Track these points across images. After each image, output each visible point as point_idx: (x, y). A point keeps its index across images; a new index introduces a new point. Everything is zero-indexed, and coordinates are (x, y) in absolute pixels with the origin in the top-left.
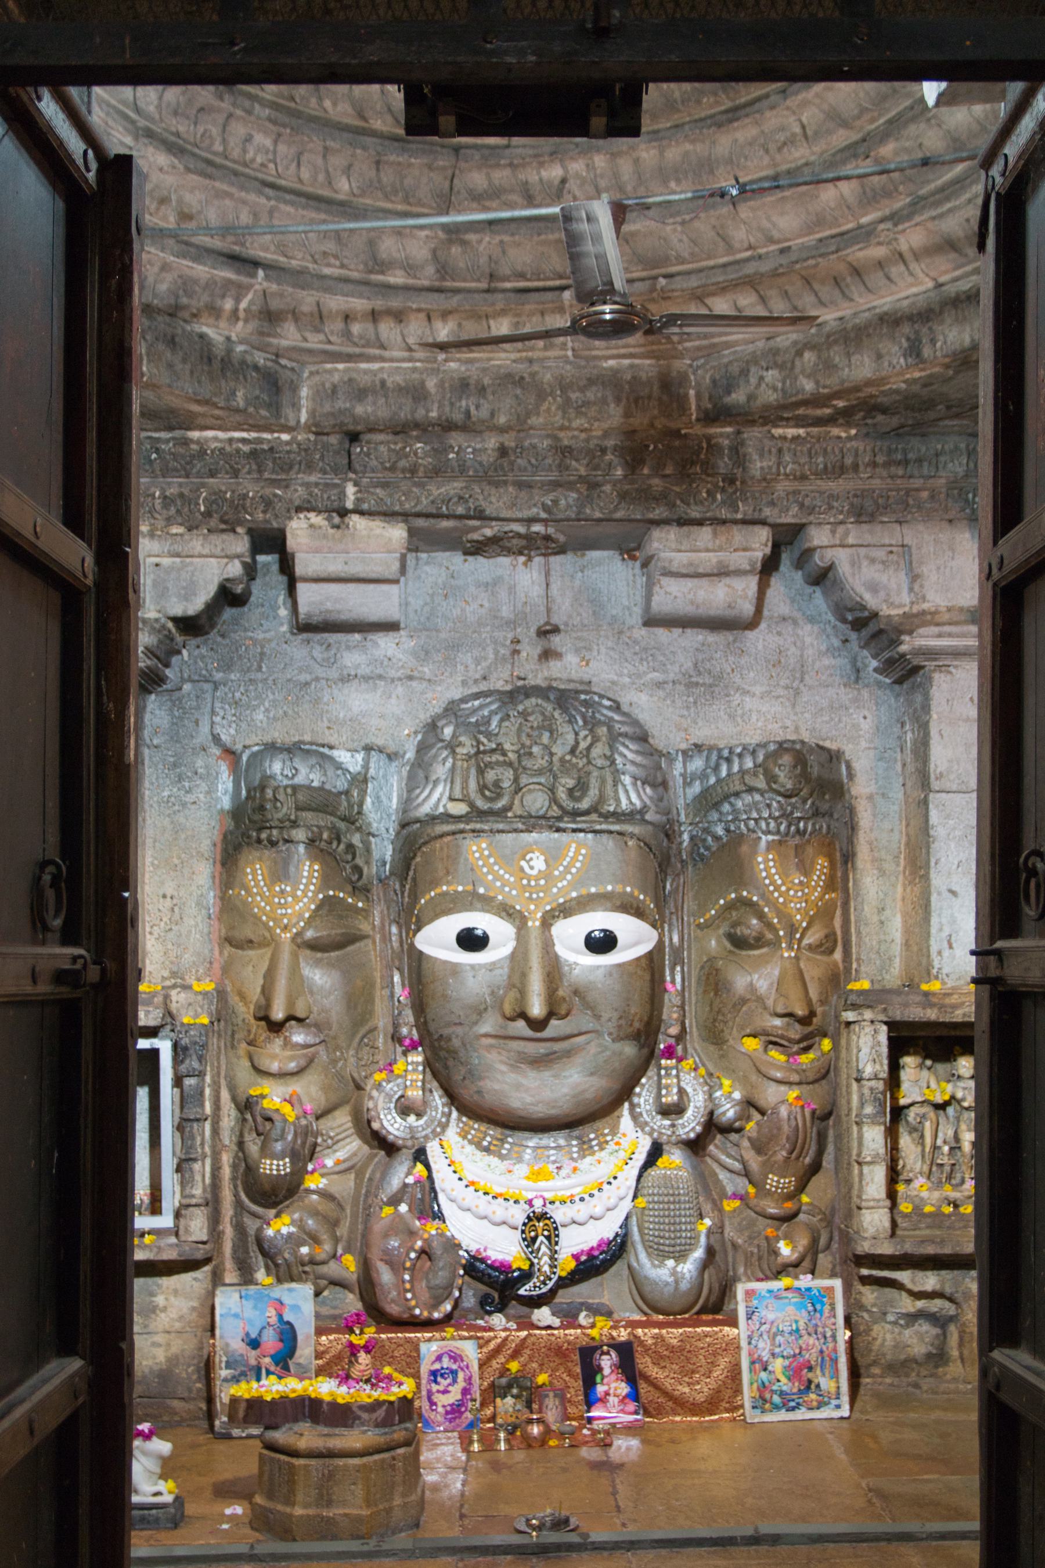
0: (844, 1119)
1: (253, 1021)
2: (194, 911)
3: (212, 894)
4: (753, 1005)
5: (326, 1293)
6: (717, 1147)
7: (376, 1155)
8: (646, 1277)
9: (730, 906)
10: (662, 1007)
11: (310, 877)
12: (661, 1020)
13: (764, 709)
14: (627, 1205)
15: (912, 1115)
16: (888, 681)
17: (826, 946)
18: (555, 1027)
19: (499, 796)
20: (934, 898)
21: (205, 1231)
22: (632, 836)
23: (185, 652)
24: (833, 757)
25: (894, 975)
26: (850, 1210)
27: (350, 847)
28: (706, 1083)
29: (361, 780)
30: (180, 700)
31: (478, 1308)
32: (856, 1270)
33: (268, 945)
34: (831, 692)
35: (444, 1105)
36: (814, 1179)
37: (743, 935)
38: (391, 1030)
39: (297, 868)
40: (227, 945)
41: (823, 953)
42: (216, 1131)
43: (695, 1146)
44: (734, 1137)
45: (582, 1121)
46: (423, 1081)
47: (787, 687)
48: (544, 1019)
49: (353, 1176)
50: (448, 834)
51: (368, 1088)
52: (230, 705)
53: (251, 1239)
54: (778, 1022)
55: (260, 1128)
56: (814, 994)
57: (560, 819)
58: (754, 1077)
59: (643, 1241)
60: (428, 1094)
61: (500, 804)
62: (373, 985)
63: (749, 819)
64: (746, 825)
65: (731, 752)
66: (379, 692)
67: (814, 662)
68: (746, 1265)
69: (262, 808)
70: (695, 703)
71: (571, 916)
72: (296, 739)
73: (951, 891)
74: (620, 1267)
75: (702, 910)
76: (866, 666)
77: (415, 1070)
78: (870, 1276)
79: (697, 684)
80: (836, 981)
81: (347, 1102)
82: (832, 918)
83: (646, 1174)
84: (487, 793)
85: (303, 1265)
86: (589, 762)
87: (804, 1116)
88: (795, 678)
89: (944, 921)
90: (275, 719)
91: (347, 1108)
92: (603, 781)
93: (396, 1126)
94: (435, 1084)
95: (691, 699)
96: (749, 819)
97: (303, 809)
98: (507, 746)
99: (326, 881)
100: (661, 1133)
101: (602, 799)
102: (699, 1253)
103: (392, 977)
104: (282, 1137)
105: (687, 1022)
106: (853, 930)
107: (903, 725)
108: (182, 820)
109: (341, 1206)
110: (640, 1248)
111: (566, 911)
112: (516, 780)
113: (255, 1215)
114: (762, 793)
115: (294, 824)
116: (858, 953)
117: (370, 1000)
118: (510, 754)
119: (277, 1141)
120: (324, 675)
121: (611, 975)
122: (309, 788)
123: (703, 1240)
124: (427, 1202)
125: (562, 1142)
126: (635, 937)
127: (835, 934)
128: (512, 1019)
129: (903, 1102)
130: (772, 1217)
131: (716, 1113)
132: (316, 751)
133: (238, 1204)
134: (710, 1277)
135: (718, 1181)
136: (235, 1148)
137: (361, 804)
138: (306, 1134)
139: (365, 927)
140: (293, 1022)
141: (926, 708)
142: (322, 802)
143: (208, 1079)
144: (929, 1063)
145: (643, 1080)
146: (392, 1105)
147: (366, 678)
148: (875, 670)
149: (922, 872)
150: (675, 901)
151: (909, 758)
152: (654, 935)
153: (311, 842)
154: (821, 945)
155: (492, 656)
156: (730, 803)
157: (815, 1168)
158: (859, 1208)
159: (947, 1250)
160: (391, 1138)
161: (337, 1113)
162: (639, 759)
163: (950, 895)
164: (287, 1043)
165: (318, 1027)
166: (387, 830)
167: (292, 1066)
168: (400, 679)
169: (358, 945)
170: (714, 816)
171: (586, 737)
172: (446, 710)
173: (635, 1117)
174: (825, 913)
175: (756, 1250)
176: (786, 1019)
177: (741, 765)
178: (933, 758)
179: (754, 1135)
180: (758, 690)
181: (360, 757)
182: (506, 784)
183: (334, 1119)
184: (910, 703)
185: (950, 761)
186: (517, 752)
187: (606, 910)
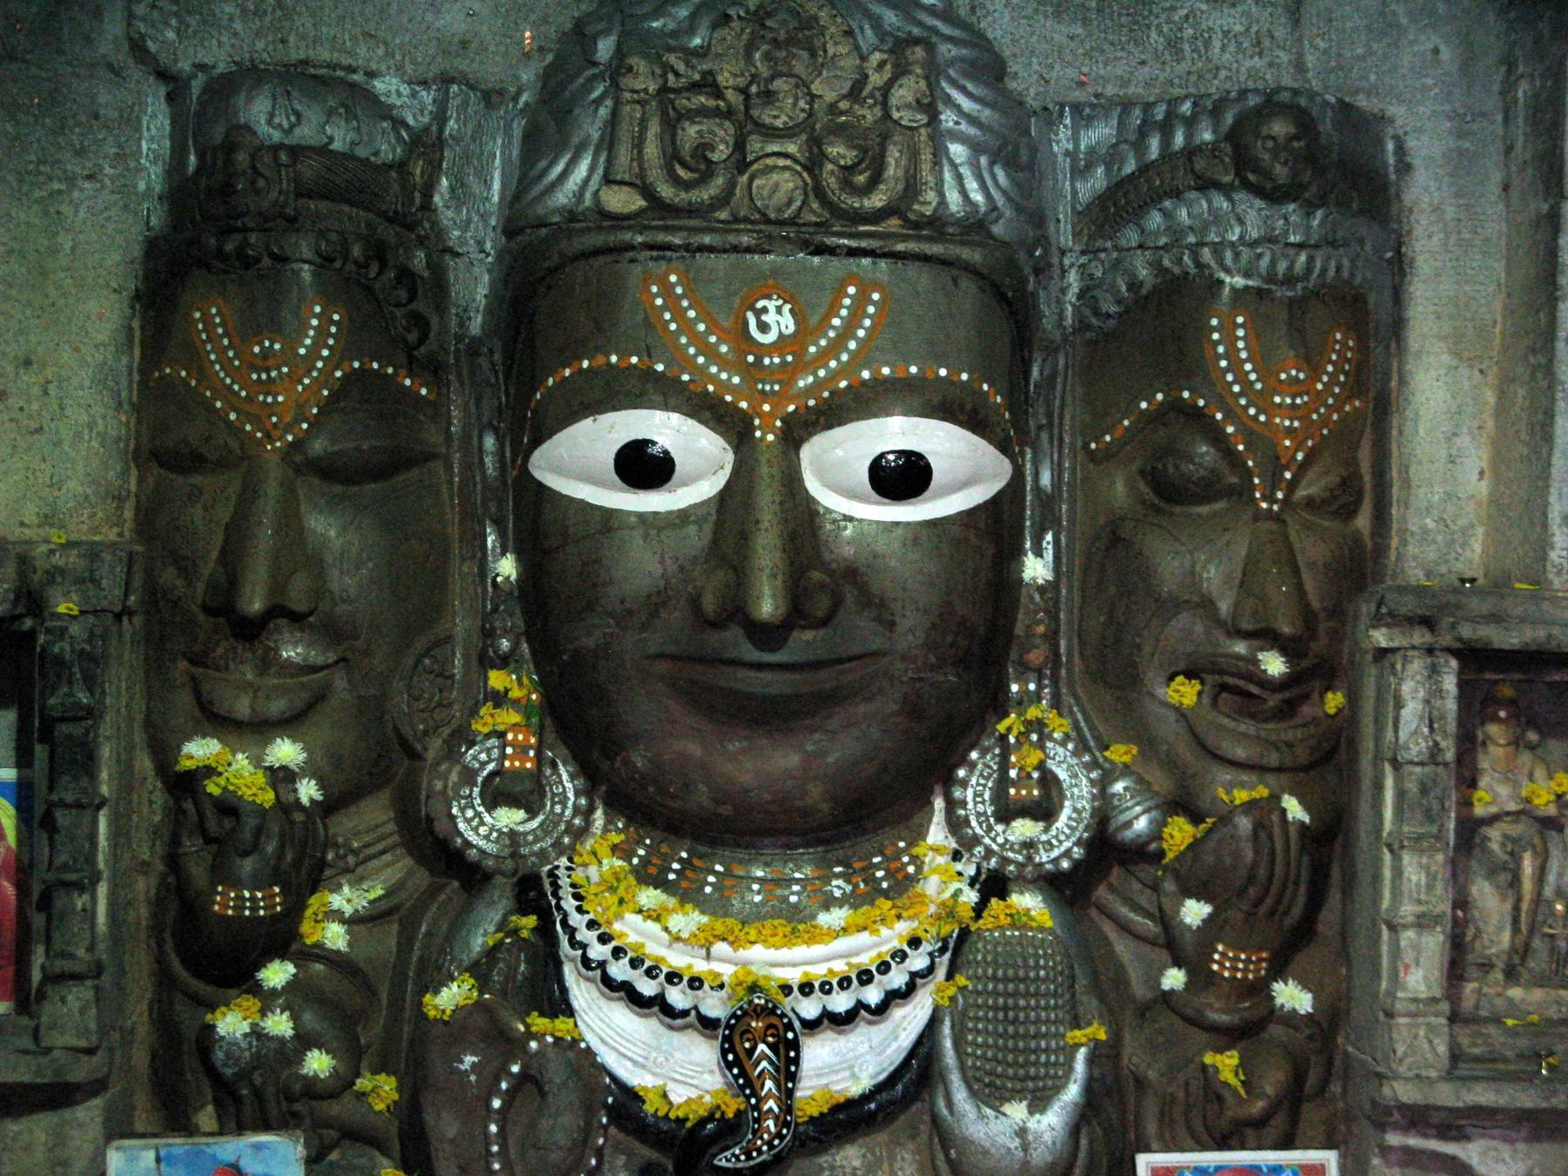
5: (334, 1156)
7: (441, 888)
9: (1157, 417)
10: (1015, 609)
11: (322, 332)
12: (1010, 636)
17: (1342, 502)
18: (803, 643)
19: (705, 177)
27: (406, 276)
29: (427, 145)
35: (577, 794)
39: (296, 312)
41: (1335, 514)
49: (395, 928)
50: (597, 252)
57: (822, 229)
59: (962, 1068)
61: (705, 194)
68: (1161, 1121)
69: (227, 190)
71: (841, 422)
72: (302, 56)
75: (1098, 421)
84: (681, 172)
86: (887, 116)
92: (914, 155)
97: (310, 195)
98: (724, 79)
99: (350, 345)
100: (1008, 861)
101: (912, 188)
109: (371, 990)
110: (955, 1080)
112: (740, 146)
118: (730, 95)
119: (246, 854)
121: (916, 541)
122: (323, 150)
129: (1479, 810)
131: (1113, 826)
132: (342, 80)
135: (1111, 954)
136: (160, 866)
137: (428, 192)
139: (433, 437)
140: (282, 622)
142: (349, 182)
146: (476, 790)
150: (1049, 404)
153: (324, 262)
156: (1167, 214)
162: (986, 114)
164: (268, 662)
166: (480, 243)
170: (1131, 236)
171: (881, 65)
174: (1342, 440)
177: (1189, 136)
182: (721, 153)
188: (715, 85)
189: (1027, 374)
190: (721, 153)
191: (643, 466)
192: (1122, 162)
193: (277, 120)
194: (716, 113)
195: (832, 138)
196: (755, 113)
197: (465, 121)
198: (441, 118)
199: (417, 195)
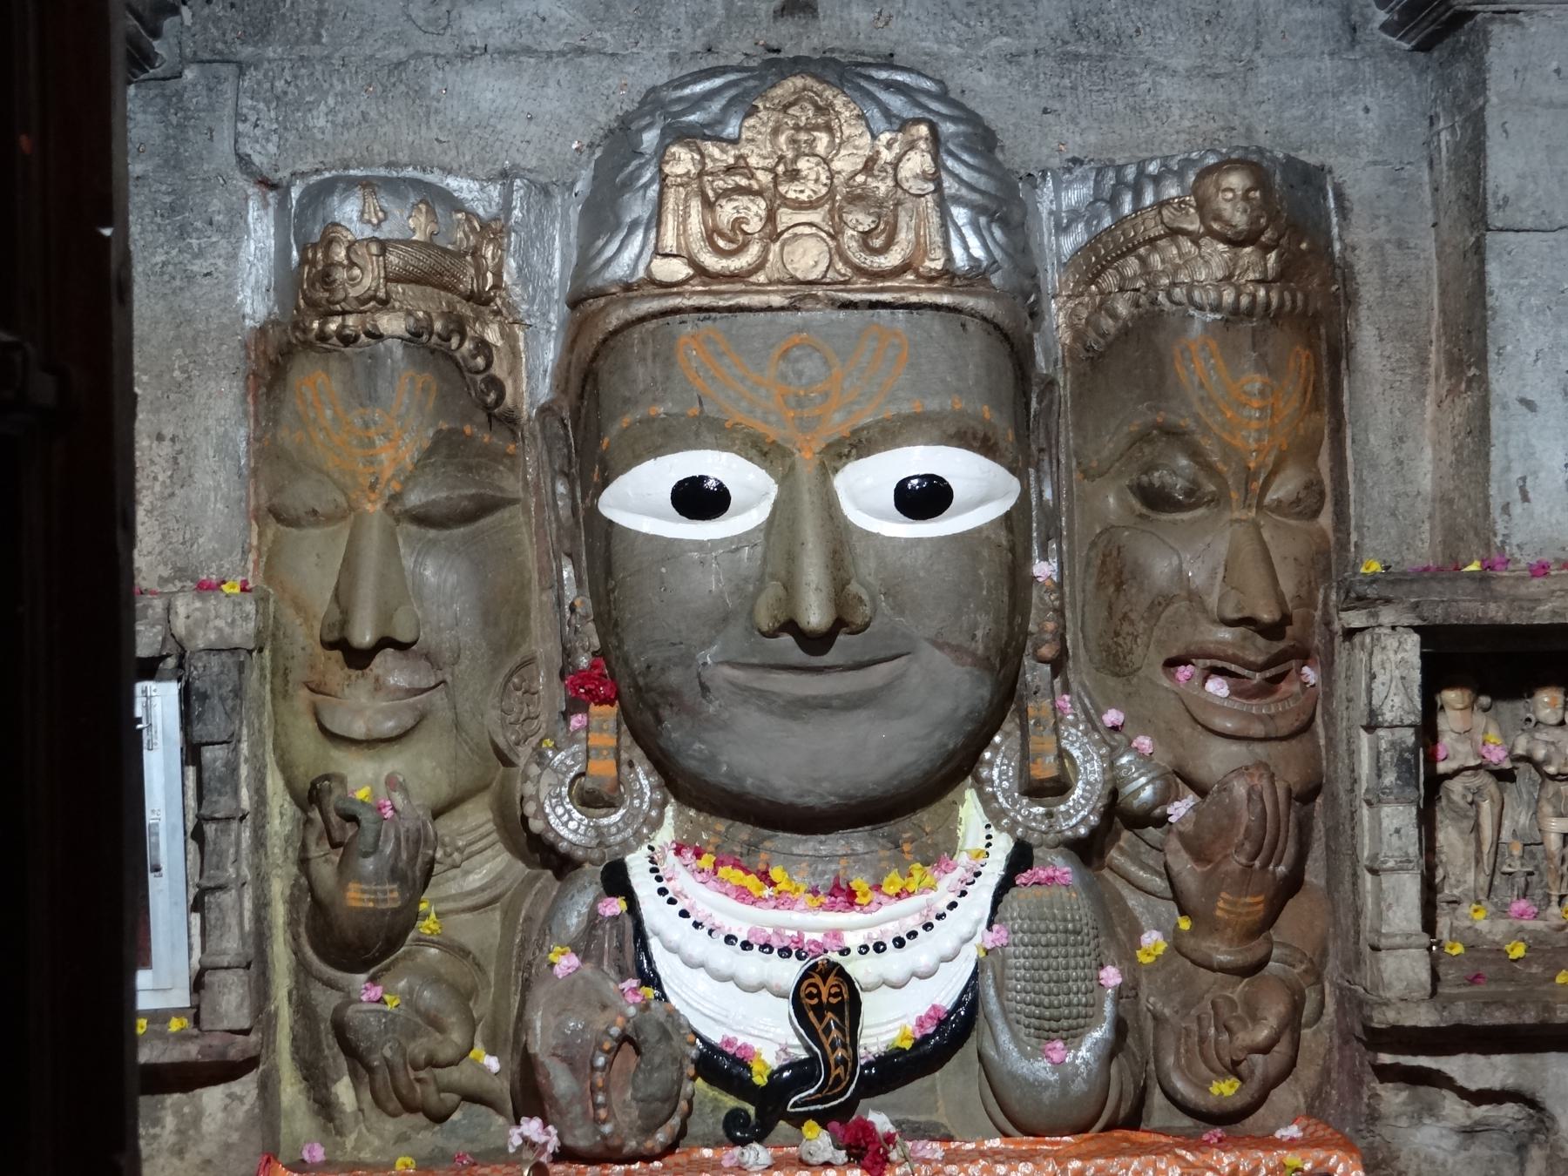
0: (1343, 798)
1: (319, 649)
2: (212, 463)
3: (243, 432)
4: (1182, 606)
6: (1122, 851)
7: (537, 878)
8: (1013, 1076)
9: (1143, 438)
13: (1194, 97)
14: (970, 955)
15: (1456, 788)
16: (1406, 46)
17: (1306, 505)
20: (1495, 415)
21: (246, 1011)
22: (973, 314)
23: (185, 10)
24: (1310, 178)
25: (1423, 550)
26: (1358, 954)
27: (483, 346)
28: (1105, 742)
30: (179, 95)
31: (721, 1132)
32: (1369, 1056)
33: (343, 518)
34: (1308, 66)
36: (1290, 902)
37: (1163, 487)
38: (558, 661)
40: (271, 520)
42: (259, 842)
43: (1087, 850)
44: (1152, 833)
45: (895, 813)
46: (617, 751)
47: (1232, 59)
48: (824, 631)
49: (497, 915)
51: (522, 762)
52: (267, 102)
53: (325, 1027)
54: (1225, 634)
55: (337, 835)
56: (1288, 586)
58: (1187, 730)
59: (1005, 1011)
60: (625, 769)
62: (524, 587)
63: (1174, 284)
64: (1169, 295)
65: (1141, 172)
66: (526, 78)
67: (1277, 14)
70: (1074, 88)
73: (1524, 402)
74: (963, 1061)
76: (1367, 21)
77: (601, 730)
78: (1395, 1067)
79: (1077, 57)
80: (1328, 561)
81: (486, 787)
82: (1315, 457)
83: (1007, 897)
84: (721, 243)
85: (416, 1068)
86: (897, 184)
87: (1275, 792)
88: (1245, 43)
89: (1513, 452)
90: (346, 125)
91: (485, 799)
92: (922, 219)
93: (573, 825)
94: (638, 752)
95: (1067, 82)
96: (1174, 284)
97: (398, 279)
98: (753, 161)
100: (1028, 828)
102: (1100, 1033)
103: (560, 572)
104: (375, 849)
105: (1068, 637)
106: (1350, 477)
107: (1432, 121)
108: (188, 305)
110: (1000, 1024)
111: (860, 445)
112: (771, 217)
113: (330, 984)
114: (1195, 239)
115: (385, 303)
116: (1360, 517)
117: (522, 610)
118: (760, 175)
119: (366, 855)
120: (430, 48)
123: (1108, 1008)
124: (633, 953)
125: (860, 847)
126: (981, 489)
127: (1320, 482)
128: (773, 634)
129: (1442, 767)
130: (1223, 969)
133: (302, 969)
134: (1120, 1072)
138: (417, 842)
139: (511, 485)
141: (1478, 85)
143: (244, 747)
144: (1485, 700)
145: (997, 739)
146: (565, 790)
147: (506, 53)
148: (1384, 27)
149: (1473, 371)
151: (1445, 174)
152: (1014, 485)
154: (1298, 501)
155: (721, 11)
157: (1293, 884)
158: (1375, 949)
159: (1530, 1017)
160: (563, 846)
161: (468, 807)
163: (1524, 410)
164: (378, 686)
165: (431, 659)
167: (389, 726)
168: (562, 53)
169: (498, 515)
172: (642, 103)
173: (987, 800)
174: (1306, 451)
175: (1195, 1027)
176: (1242, 629)
177: (1157, 193)
178: (1491, 173)
179: (1188, 827)
180: (1180, 63)
181: (495, 191)
183: (464, 816)
184: (1446, 81)
185: (1521, 177)
186: (772, 170)
187: (926, 444)
188: (747, 166)
189: (1027, 405)
190: (754, 226)
191: (699, 499)
192: (1099, 218)
193: (366, 216)
194: (747, 191)
195: (850, 207)
196: (782, 189)
197: (528, 211)
198: (507, 207)
199: (489, 275)
